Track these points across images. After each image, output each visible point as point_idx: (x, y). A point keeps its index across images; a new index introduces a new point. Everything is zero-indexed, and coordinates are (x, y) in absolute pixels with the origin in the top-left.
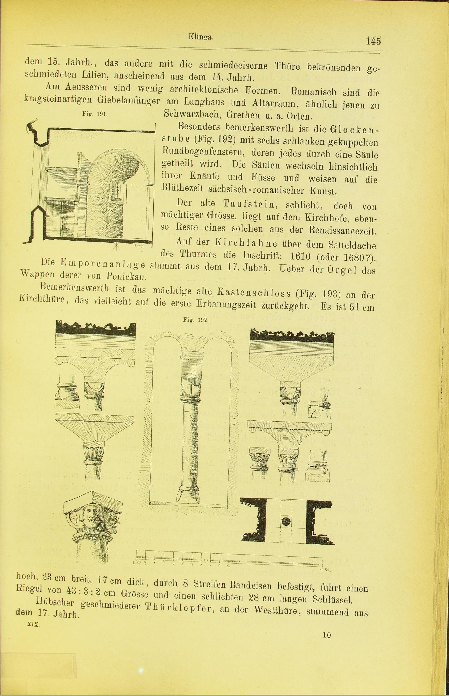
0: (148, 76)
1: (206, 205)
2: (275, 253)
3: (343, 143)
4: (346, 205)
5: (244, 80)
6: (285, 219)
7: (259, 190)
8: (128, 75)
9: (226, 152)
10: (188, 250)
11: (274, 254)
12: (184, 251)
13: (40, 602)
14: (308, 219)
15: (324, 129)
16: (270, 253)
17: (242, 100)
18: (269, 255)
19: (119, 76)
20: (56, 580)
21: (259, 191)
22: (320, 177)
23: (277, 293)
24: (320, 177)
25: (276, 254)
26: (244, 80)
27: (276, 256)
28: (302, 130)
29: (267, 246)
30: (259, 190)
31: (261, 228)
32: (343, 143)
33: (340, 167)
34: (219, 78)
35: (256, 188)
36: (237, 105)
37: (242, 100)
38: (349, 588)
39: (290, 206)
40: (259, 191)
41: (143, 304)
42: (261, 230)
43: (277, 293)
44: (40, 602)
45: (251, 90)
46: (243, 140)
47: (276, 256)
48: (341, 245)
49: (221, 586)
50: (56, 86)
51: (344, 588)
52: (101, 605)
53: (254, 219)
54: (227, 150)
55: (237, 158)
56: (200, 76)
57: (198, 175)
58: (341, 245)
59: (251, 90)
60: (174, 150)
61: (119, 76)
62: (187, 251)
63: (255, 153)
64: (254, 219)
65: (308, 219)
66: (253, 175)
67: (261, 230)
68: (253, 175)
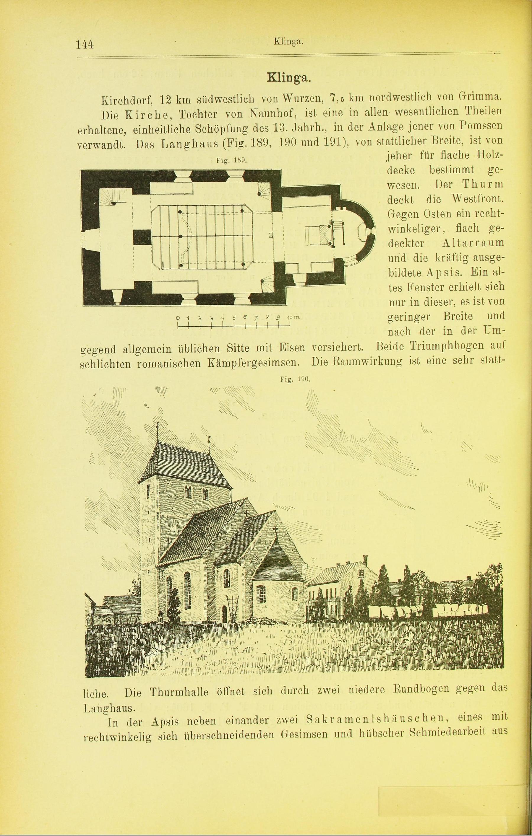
0: (438, 360)
1: (102, 134)
3: (383, 362)
7: (145, 364)
8: (85, 364)
9: (410, 97)
10: (474, 106)
12: (155, 689)
14: (211, 365)
15: (444, 360)
19: (163, 364)
20: (438, 114)
21: (145, 366)
28: (412, 362)
30: (145, 364)
31: (278, 361)
32: (383, 362)
33: (393, 361)
38: (429, 360)
39: (285, 364)
40: (145, 366)
41: (499, 347)
45: (413, 288)
48: (498, 359)
49: (214, 350)
51: (450, 361)
54: (412, 95)
58: (498, 359)
59: (413, 288)
60: (390, 361)
61: (163, 364)
62: (473, 107)
65: (211, 365)
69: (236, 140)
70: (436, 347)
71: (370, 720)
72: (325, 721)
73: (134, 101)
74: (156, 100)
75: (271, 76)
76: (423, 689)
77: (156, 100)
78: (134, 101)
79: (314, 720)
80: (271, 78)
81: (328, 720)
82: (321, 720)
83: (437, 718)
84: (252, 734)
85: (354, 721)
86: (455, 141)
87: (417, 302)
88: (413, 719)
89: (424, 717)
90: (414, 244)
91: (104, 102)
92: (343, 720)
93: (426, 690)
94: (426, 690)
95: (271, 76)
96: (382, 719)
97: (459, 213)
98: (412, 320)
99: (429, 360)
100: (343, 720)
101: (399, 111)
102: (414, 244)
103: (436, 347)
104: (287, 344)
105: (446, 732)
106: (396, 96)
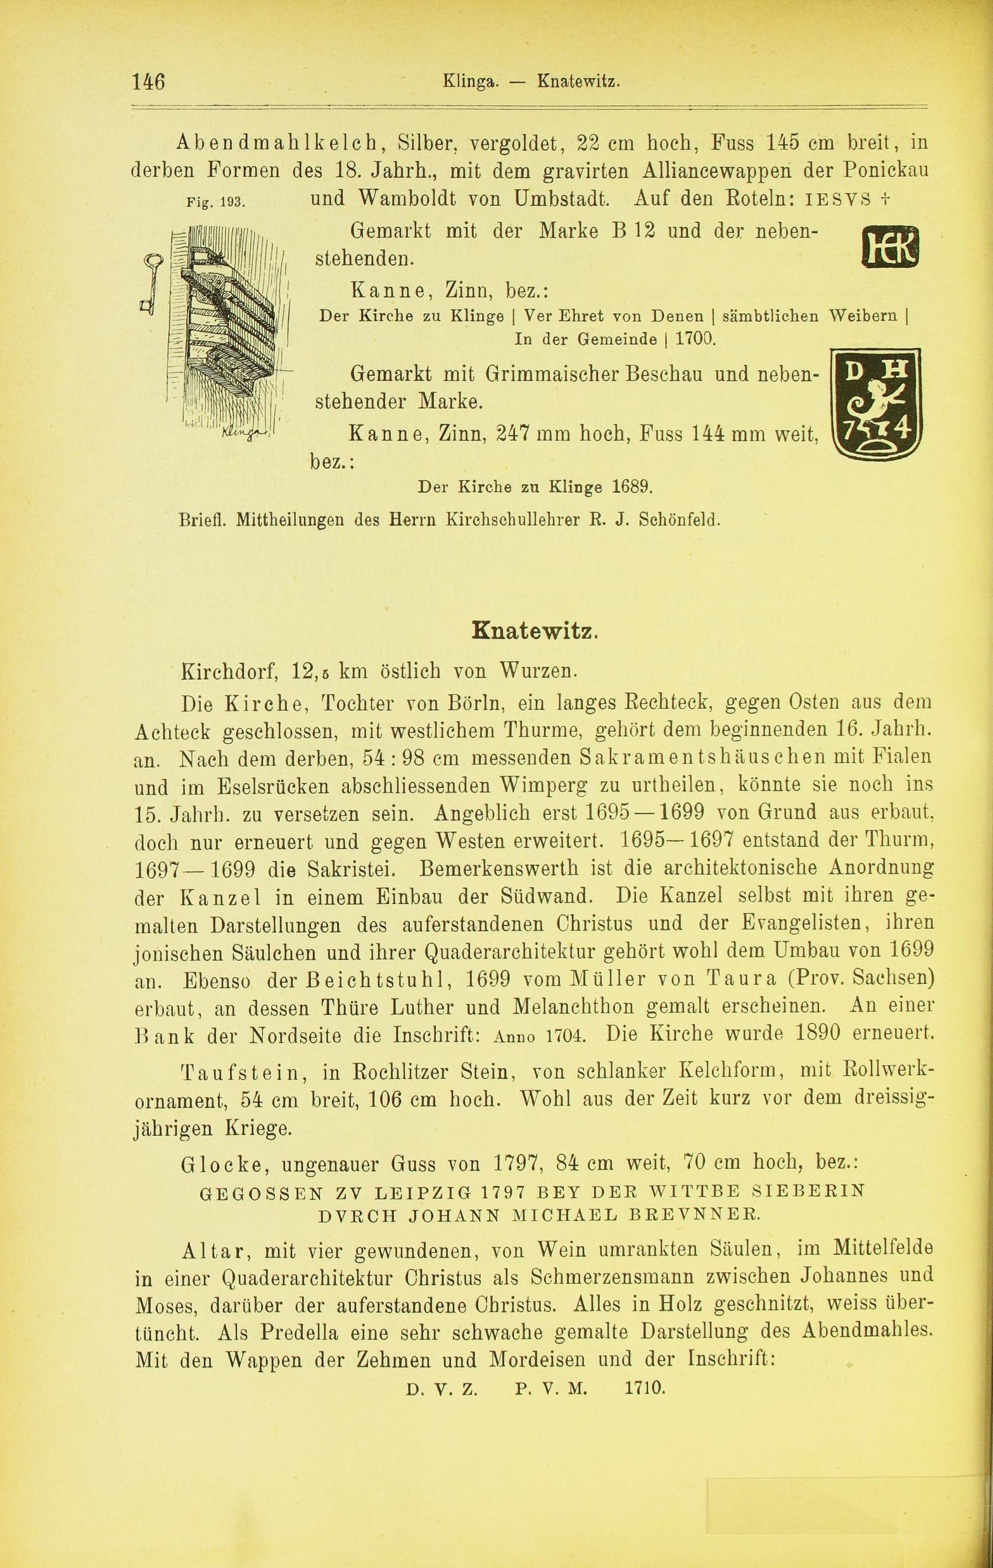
2: (760, 1353)
4: (781, 1160)
5: (435, 1339)
6: (650, 1363)
11: (758, 1355)
13: (667, 1306)
16: (454, 1030)
17: (350, 947)
18: (508, 1303)
22: (884, 1092)
23: (215, 1165)
24: (884, 1092)
25: (761, 1353)
26: (435, 1339)
27: (761, 1358)
29: (403, 296)
34: (578, 1038)
35: (395, 950)
36: (480, 1013)
37: (350, 947)
42: (708, 202)
43: (215, 1165)
44: (667, 1306)
46: (449, 374)
47: (761, 1358)
50: (768, 1069)
52: (896, 1061)
53: (734, 736)
55: (619, 1019)
56: (672, 1004)
57: (848, 865)
63: (255, 1009)
64: (734, 736)
66: (211, 166)
67: (708, 202)
68: (211, 166)
69: (889, 751)
70: (428, 1102)
71: (696, 758)
72: (612, 761)
73: (243, 672)
74: (284, 670)
75: (480, 627)
76: (429, 144)
77: (284, 670)
78: (243, 672)
79: (593, 761)
80: (480, 631)
81: (619, 759)
82: (606, 759)
83: (681, 758)
84: (924, 754)
85: (666, 759)
86: (718, 868)
87: (645, 1304)
88: (772, 758)
89: (453, 1098)
90: (676, 1249)
91: (186, 674)
92: (646, 758)
93: (378, 1075)
94: (378, 1075)
95: (480, 627)
96: (718, 757)
97: (747, 839)
98: (734, 1337)
99: (311, 1332)
100: (646, 758)
101: (835, 1300)
102: (676, 1249)
103: (428, 1102)
104: (888, 750)
105: (190, 733)
106: (889, 1066)
